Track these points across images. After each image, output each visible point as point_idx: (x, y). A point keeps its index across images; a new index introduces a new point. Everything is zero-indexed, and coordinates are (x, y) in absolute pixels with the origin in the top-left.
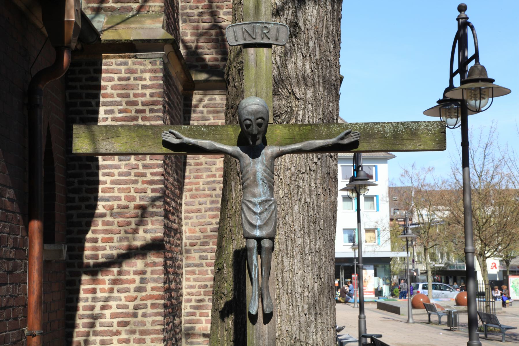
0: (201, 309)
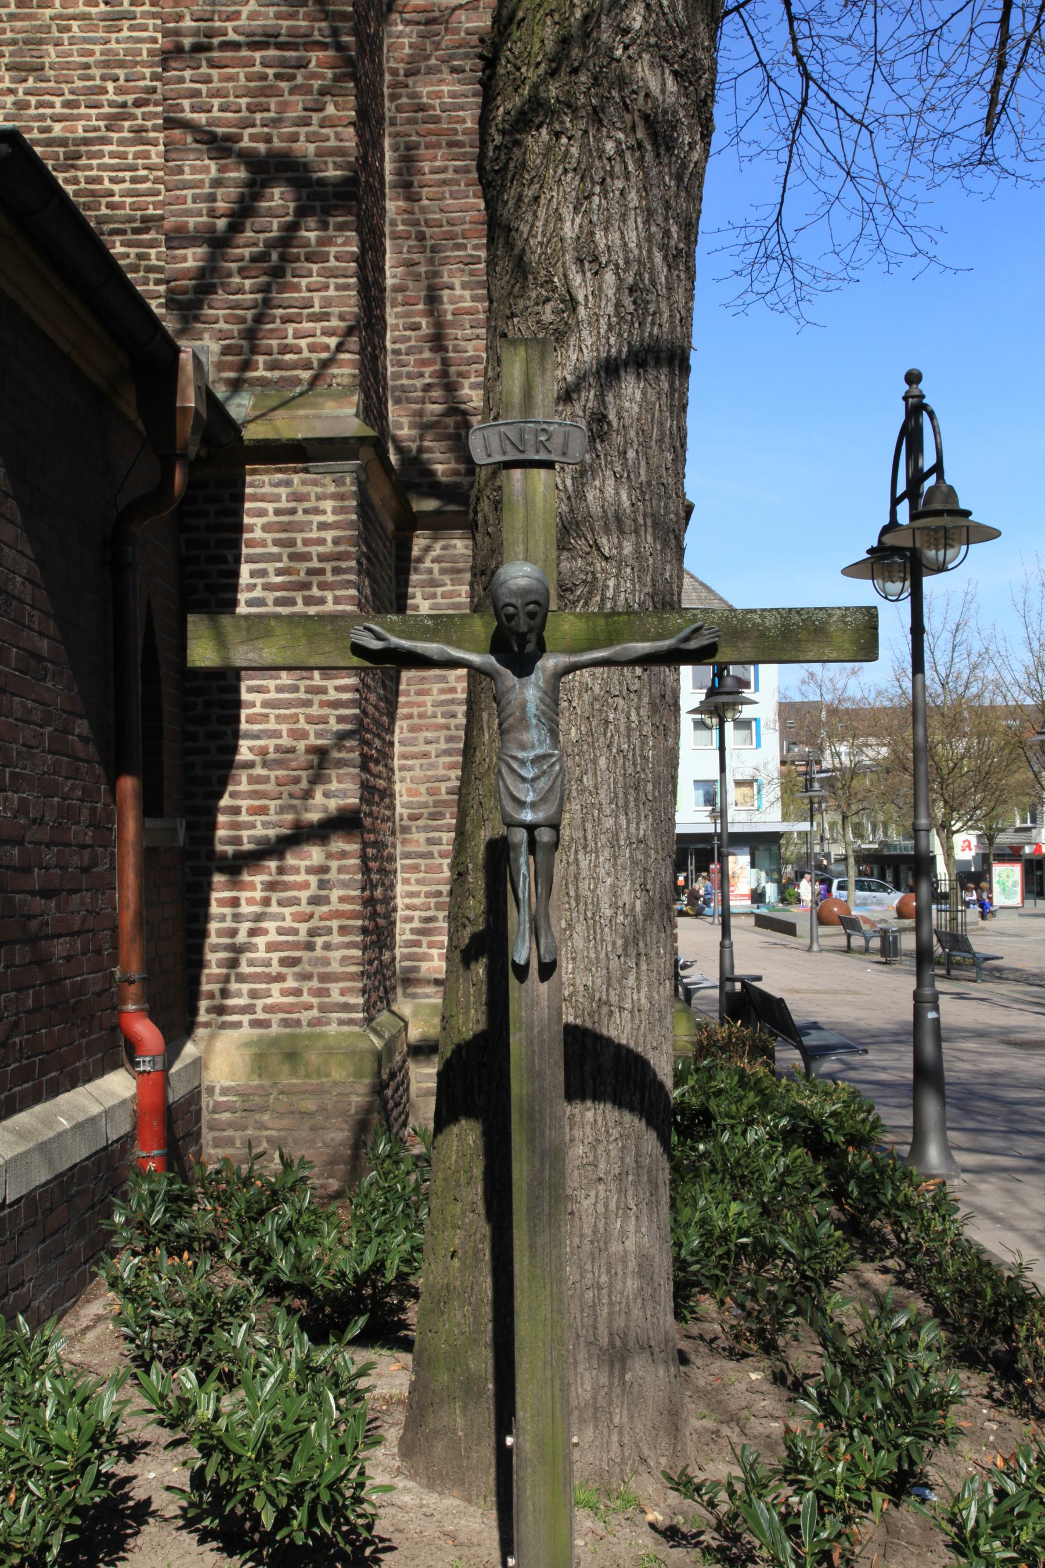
0: (430, 935)
